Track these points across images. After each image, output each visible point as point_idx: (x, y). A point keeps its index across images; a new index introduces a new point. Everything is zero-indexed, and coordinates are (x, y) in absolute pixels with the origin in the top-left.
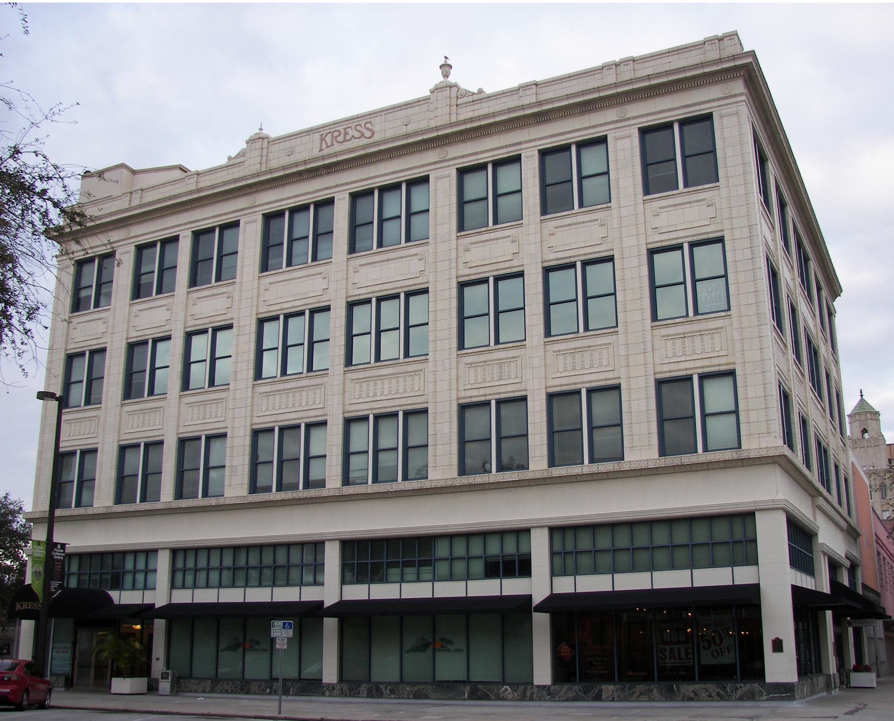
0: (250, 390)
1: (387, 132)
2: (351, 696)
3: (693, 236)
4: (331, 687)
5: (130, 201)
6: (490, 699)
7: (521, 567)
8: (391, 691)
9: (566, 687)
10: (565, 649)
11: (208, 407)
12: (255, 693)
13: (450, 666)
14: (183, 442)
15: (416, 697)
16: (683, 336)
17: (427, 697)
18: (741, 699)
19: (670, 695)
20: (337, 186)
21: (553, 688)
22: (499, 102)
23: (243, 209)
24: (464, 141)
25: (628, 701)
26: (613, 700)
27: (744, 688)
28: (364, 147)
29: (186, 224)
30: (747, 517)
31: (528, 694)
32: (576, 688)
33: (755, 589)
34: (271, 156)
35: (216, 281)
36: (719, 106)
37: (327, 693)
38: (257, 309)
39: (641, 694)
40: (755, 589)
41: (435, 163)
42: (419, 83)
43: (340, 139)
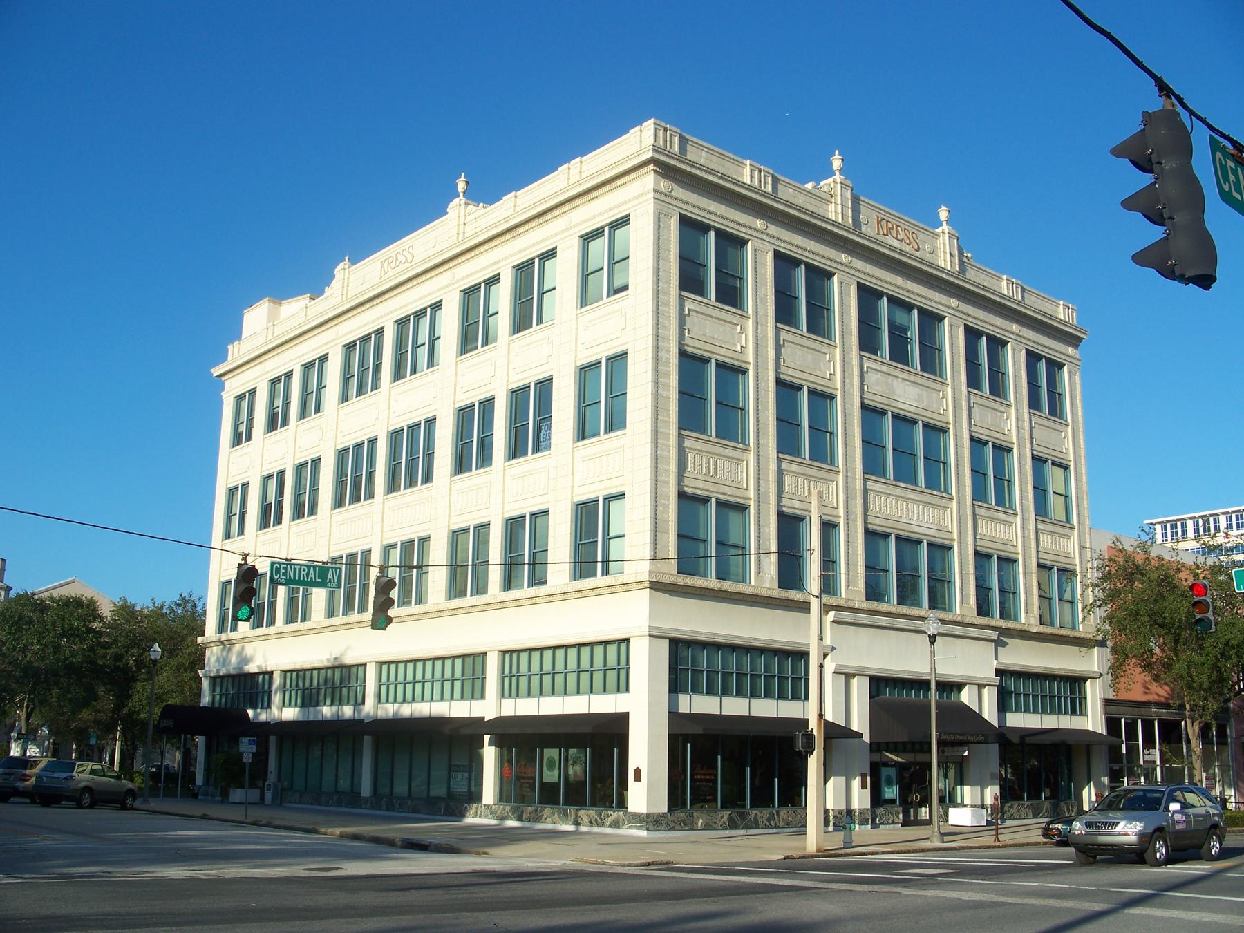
7: (475, 690)
27: (614, 815)
28: (901, 252)
43: (393, 265)
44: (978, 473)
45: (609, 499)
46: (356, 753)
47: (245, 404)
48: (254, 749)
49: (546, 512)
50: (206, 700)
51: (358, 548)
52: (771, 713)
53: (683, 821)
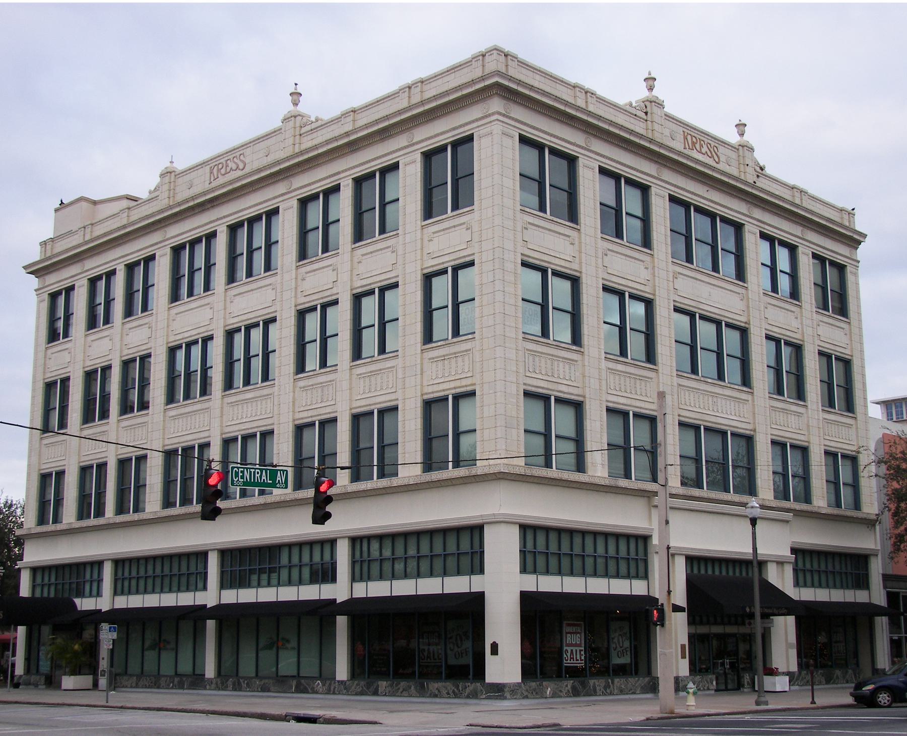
0: (419, 356)
1: (256, 161)
2: (223, 690)
3: (454, 260)
4: (210, 680)
5: (409, 97)
6: (308, 693)
7: (327, 574)
8: (247, 684)
9: (356, 682)
10: (360, 647)
11: (259, 403)
12: (163, 688)
13: (287, 664)
14: (357, 419)
15: (263, 690)
16: (444, 358)
17: (269, 691)
18: (468, 697)
19: (422, 692)
20: (218, 219)
21: (348, 683)
22: (329, 129)
23: (156, 244)
24: (303, 172)
25: (395, 696)
26: (385, 695)
27: (471, 686)
29: (120, 258)
30: (476, 531)
31: (332, 688)
32: (362, 683)
33: (479, 598)
34: (178, 189)
35: (380, 234)
36: (478, 127)
37: (208, 687)
38: (225, 322)
39: (404, 690)
40: (479, 598)
41: (406, 147)
42: (269, 114)
43: (223, 171)
44: (828, 384)
45: (457, 398)
46: (198, 634)
47: (61, 300)
48: (115, 635)
49: (395, 409)
50: (25, 591)
51: (194, 440)
52: (138, 604)
53: (535, 690)
